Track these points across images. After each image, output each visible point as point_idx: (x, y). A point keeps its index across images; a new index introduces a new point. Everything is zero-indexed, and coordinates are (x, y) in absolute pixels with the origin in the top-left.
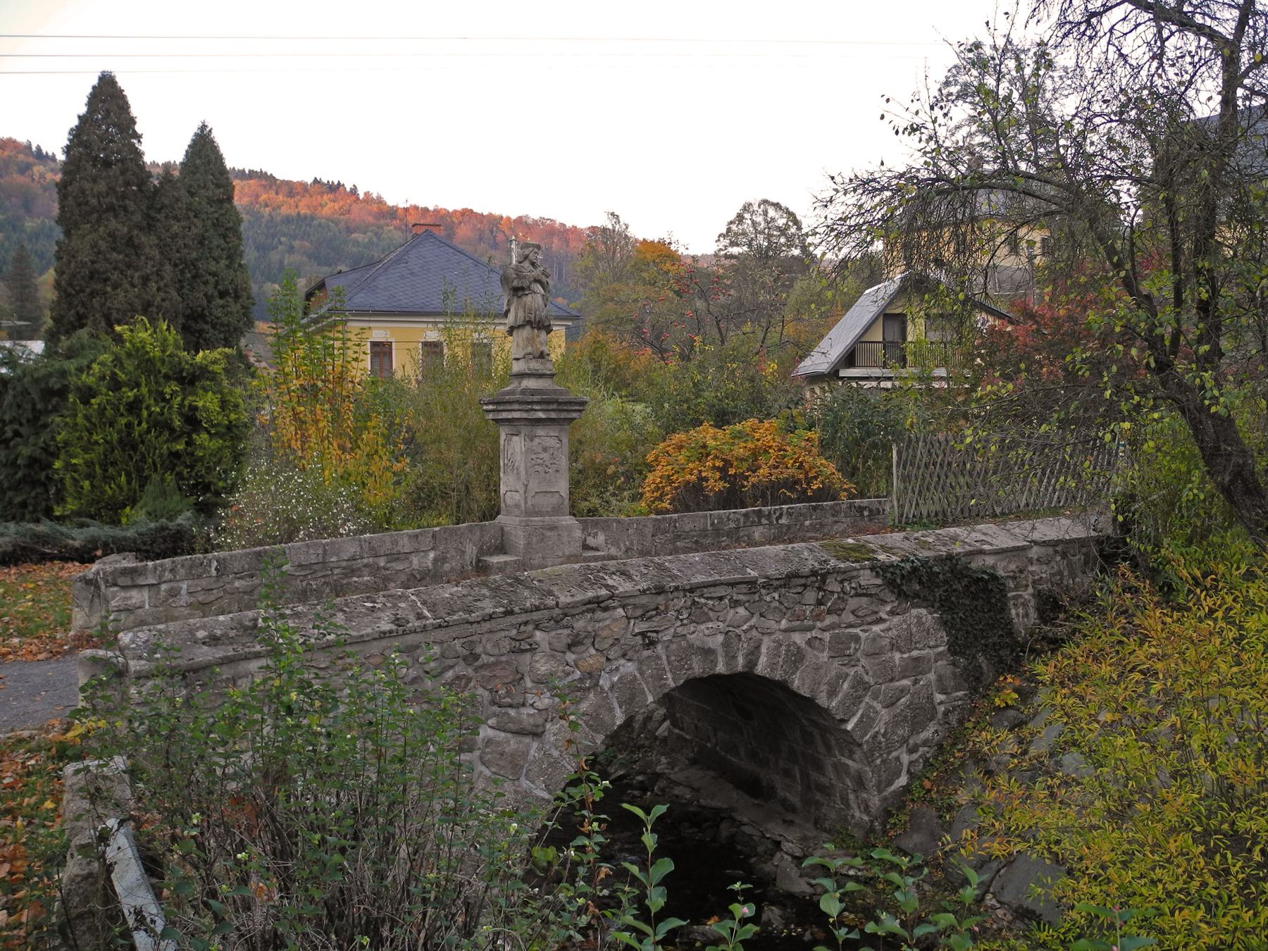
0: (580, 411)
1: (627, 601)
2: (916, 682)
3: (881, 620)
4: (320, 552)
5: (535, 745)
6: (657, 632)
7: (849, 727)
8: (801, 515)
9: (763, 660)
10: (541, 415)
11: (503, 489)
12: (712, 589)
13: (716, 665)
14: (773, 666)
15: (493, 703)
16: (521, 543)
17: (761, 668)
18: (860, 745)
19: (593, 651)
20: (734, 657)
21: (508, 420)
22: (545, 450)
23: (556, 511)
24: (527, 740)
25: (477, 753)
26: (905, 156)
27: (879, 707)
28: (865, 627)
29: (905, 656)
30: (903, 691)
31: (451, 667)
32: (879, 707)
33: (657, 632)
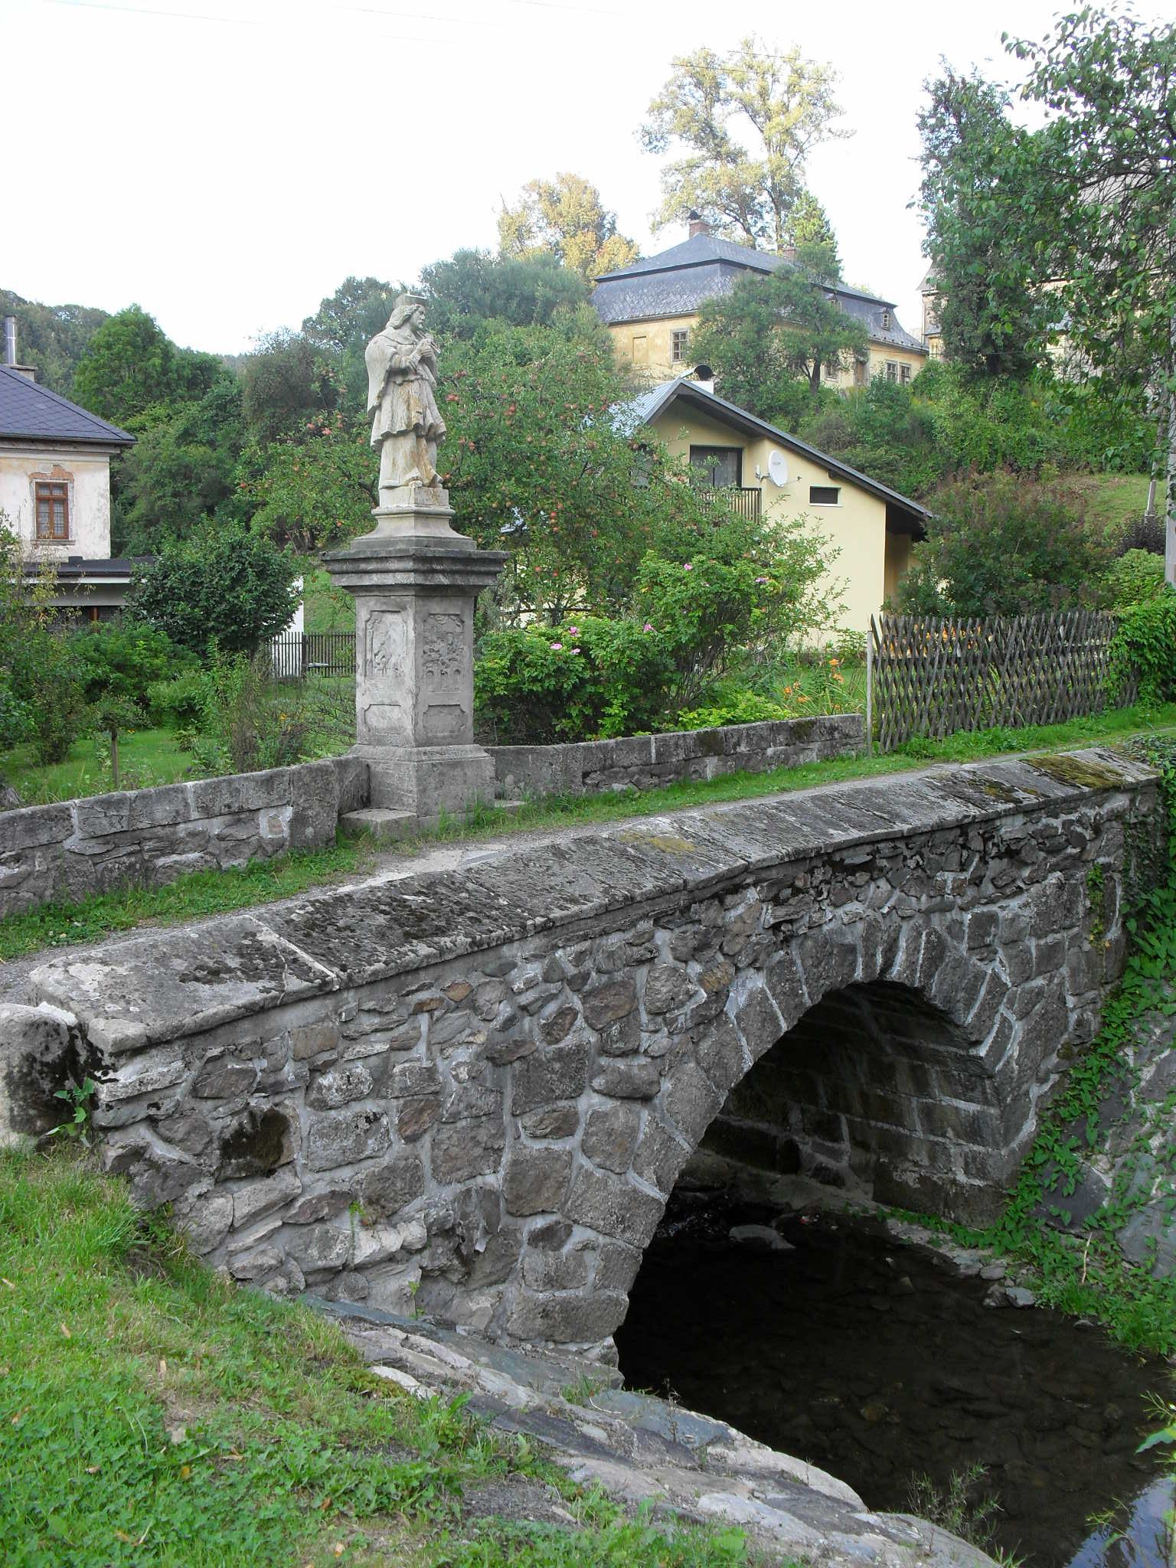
0: (494, 574)
1: (764, 875)
2: (1050, 981)
3: (1020, 891)
4: (125, 812)
5: (645, 1115)
6: (791, 922)
7: (982, 1052)
8: (762, 737)
9: (901, 957)
10: (444, 580)
11: (361, 702)
12: (851, 852)
13: (854, 971)
14: (911, 965)
15: (604, 1051)
16: (411, 785)
17: (896, 972)
18: (990, 1077)
19: (721, 958)
20: (874, 955)
21: (378, 587)
22: (442, 637)
23: (456, 739)
24: (637, 1106)
25: (579, 1135)
26: (488, 243)
27: (1012, 1018)
28: (1003, 903)
29: (1042, 942)
30: (1040, 993)
31: (553, 997)
32: (1012, 1018)
33: (791, 922)
